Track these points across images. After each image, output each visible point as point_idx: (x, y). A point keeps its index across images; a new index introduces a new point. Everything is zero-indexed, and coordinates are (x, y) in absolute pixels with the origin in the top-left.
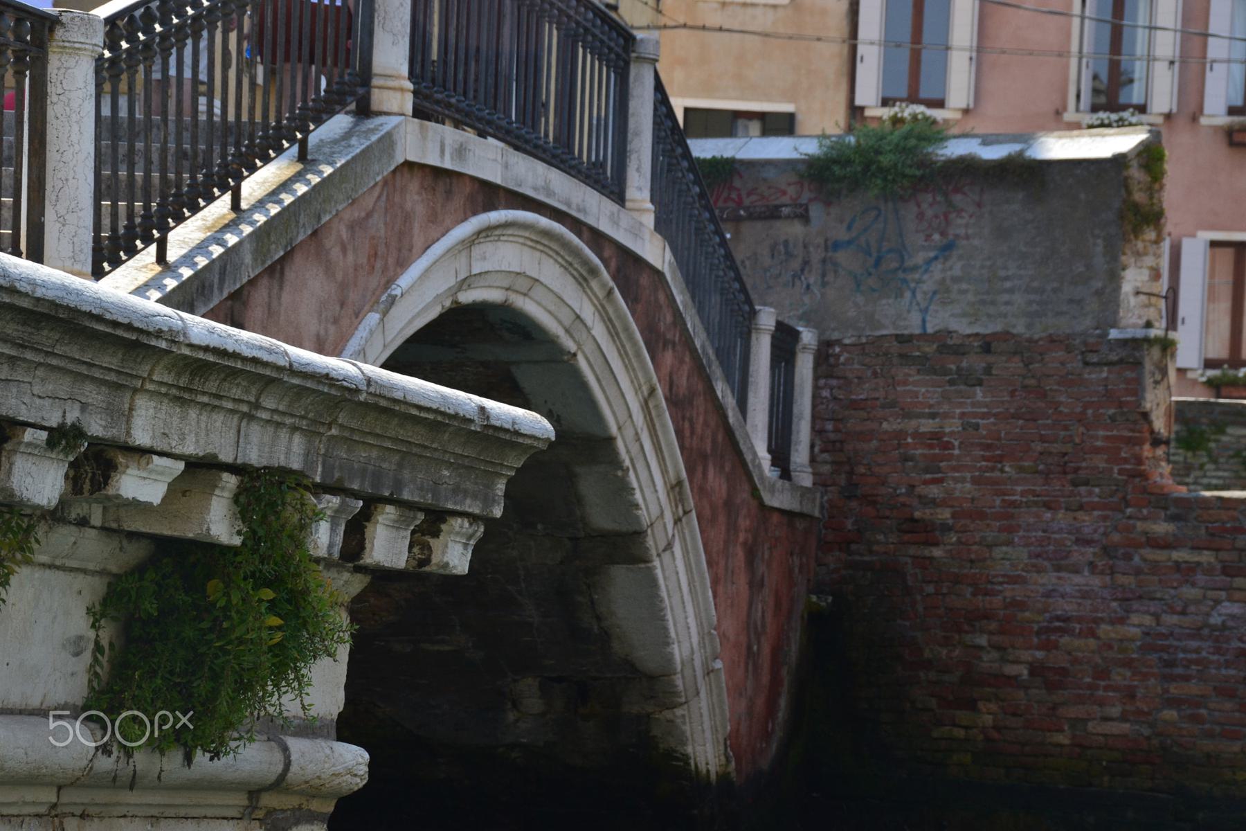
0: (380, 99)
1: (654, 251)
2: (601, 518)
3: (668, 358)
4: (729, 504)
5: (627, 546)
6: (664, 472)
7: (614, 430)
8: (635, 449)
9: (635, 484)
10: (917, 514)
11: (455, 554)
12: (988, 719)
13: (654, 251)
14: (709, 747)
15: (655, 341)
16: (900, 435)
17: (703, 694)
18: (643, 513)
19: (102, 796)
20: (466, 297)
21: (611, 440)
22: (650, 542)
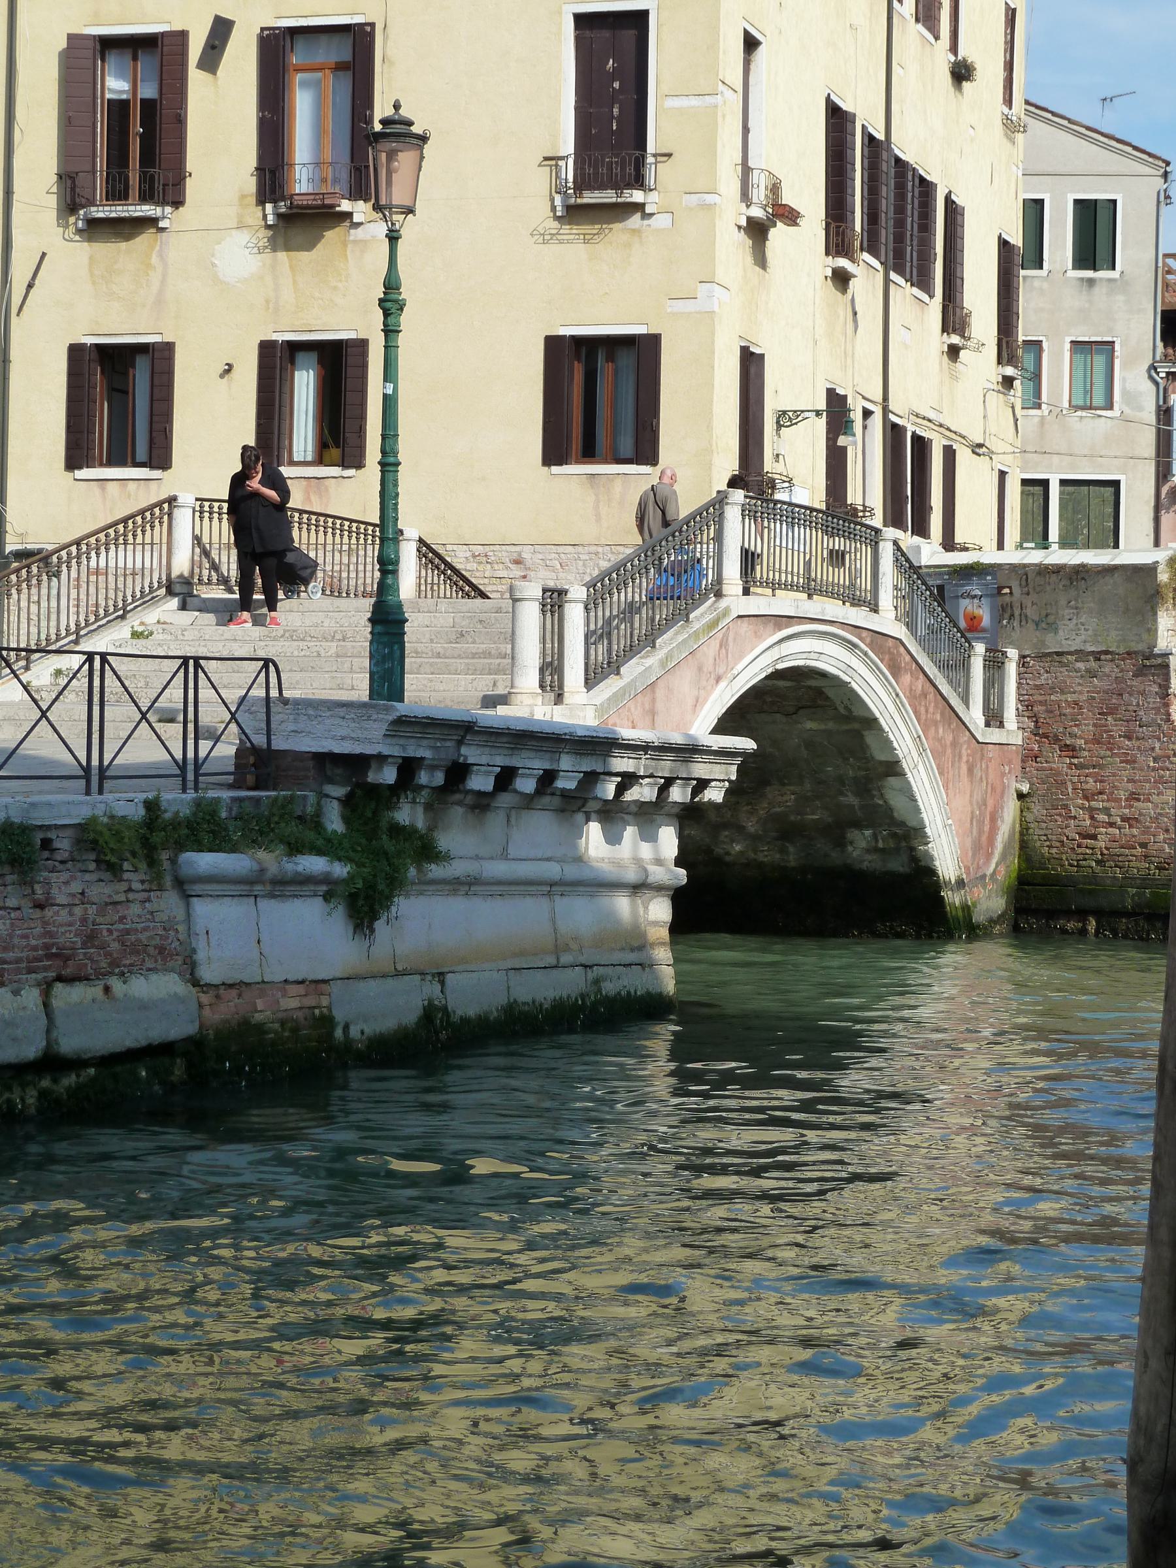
0: (726, 589)
1: (899, 631)
2: (881, 757)
3: (907, 678)
4: (954, 744)
5: (893, 768)
6: (910, 732)
7: (878, 715)
8: (891, 722)
9: (892, 738)
10: (1068, 742)
11: (715, 794)
12: (1103, 845)
13: (899, 631)
14: (949, 861)
15: (895, 670)
16: (1058, 703)
17: (943, 836)
18: (898, 752)
19: (568, 889)
20: (780, 666)
21: (876, 719)
22: (905, 765)
